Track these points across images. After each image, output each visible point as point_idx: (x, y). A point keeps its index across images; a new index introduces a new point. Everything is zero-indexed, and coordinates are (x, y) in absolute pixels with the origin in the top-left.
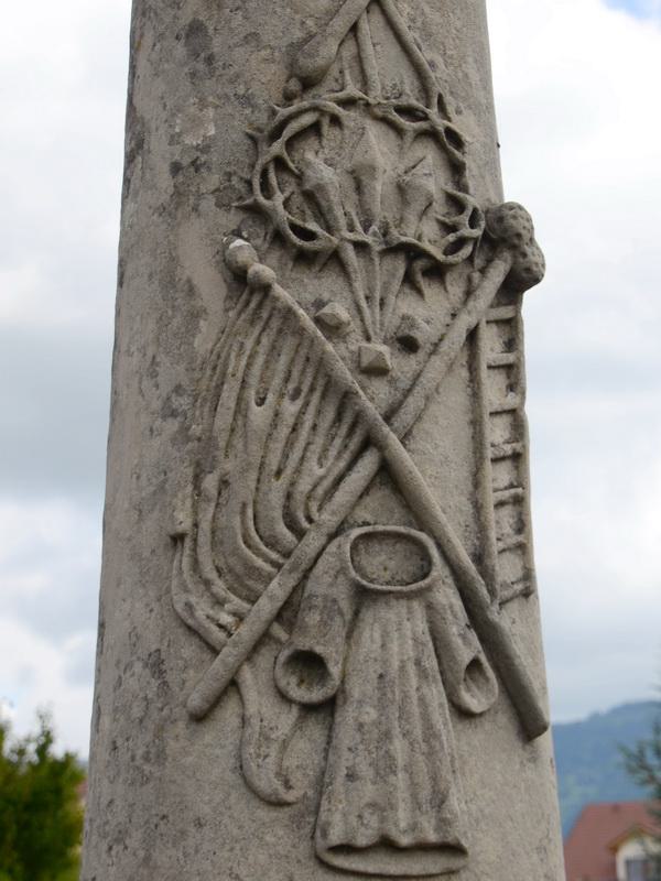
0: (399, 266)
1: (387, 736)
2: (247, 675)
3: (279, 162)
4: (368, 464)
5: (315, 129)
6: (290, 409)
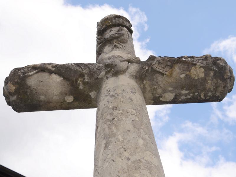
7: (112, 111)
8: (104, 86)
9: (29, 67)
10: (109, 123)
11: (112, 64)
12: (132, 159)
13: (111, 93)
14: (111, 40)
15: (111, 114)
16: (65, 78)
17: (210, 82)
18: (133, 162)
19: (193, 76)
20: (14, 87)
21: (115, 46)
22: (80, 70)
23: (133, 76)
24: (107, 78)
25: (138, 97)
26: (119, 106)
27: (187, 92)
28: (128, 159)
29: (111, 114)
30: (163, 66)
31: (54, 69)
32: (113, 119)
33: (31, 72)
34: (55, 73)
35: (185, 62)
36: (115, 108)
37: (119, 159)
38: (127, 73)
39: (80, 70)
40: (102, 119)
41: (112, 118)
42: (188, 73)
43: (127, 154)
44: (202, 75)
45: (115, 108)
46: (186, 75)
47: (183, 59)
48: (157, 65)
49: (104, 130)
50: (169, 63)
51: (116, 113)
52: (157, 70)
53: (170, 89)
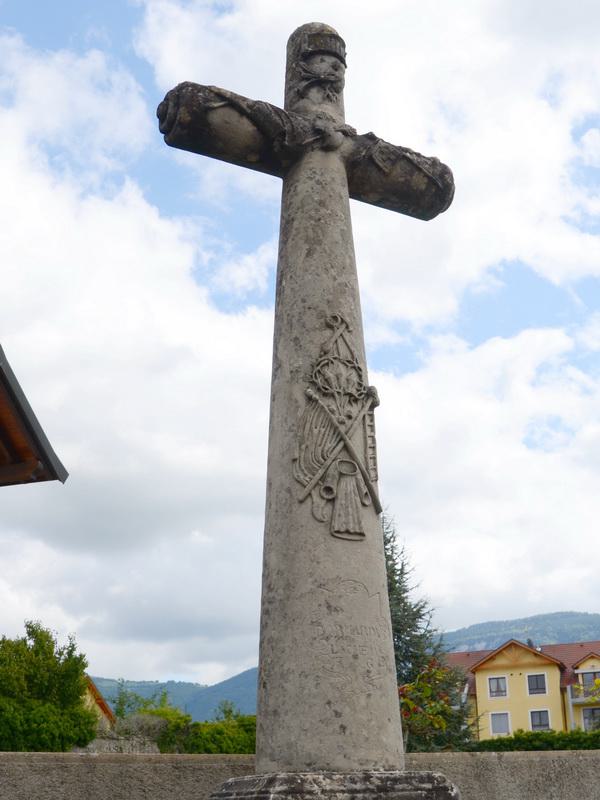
0: (347, 398)
1: (347, 507)
2: (313, 492)
3: (319, 371)
4: (341, 444)
5: (327, 364)
6: (323, 430)
7: (318, 207)
8: (306, 159)
9: (212, 91)
10: (313, 222)
11: (325, 132)
12: (339, 280)
13: (317, 177)
14: (558, 665)
15: (317, 210)
16: (258, 129)
17: (427, 198)
18: (339, 284)
19: (413, 184)
20: (189, 118)
21: (328, 96)
22: (280, 122)
23: (344, 157)
24: (313, 150)
25: (345, 191)
26: (327, 203)
27: (397, 200)
28: (335, 279)
29: (317, 210)
30: (384, 157)
31: (249, 111)
32: (319, 220)
33: (215, 102)
34: (249, 117)
35: (409, 161)
36: (322, 203)
37: (325, 276)
38: (338, 151)
39: (280, 122)
40: (303, 212)
41: (317, 217)
42: (409, 178)
43: (333, 272)
44: (423, 187)
45: (322, 203)
46: (406, 180)
47: (408, 154)
48: (377, 154)
49: (306, 229)
50: (393, 157)
51: (323, 211)
52: (377, 161)
53: (380, 190)
